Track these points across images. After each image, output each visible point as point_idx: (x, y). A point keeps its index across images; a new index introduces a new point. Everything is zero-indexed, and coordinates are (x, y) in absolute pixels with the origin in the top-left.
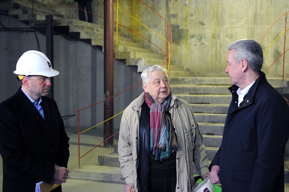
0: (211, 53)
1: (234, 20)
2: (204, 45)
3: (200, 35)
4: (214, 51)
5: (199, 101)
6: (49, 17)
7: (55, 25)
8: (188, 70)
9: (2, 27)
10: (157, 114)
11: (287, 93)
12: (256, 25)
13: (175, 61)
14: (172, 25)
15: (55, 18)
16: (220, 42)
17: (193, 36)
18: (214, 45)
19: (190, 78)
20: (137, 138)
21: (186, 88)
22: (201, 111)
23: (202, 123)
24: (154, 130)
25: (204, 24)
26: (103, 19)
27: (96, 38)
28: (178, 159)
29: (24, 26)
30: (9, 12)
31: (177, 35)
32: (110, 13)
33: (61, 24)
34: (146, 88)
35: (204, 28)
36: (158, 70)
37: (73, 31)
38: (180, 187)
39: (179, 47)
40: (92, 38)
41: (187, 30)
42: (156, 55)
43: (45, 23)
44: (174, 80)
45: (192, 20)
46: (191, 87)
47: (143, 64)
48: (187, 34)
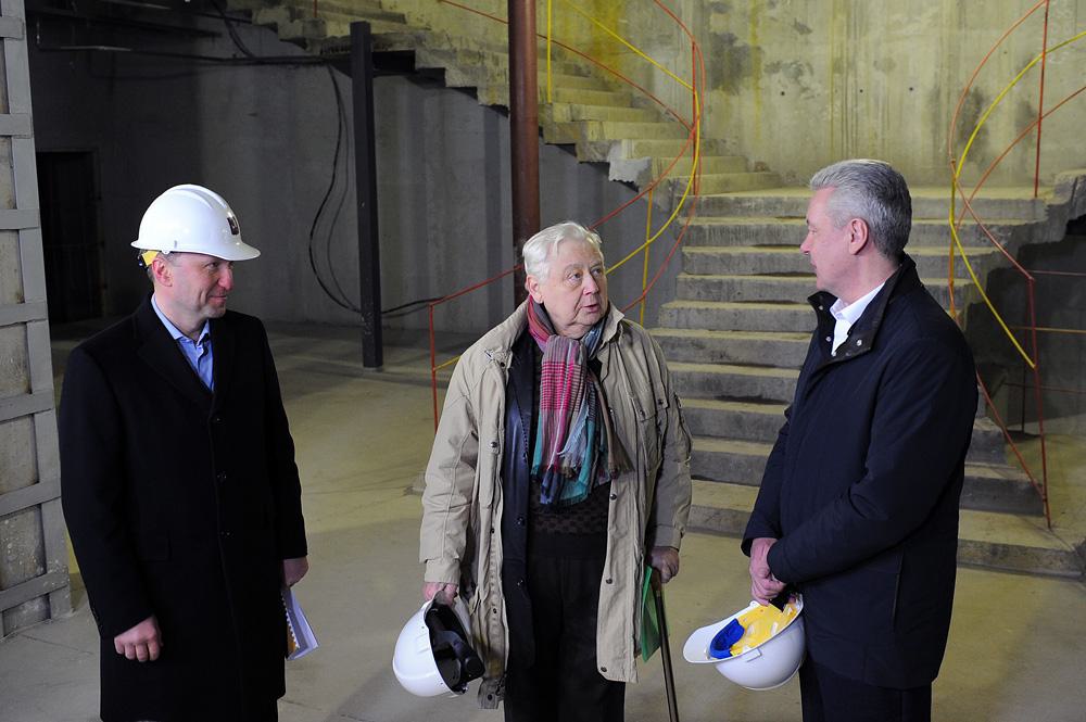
0: (830, 118)
1: (898, 16)
2: (809, 93)
3: (795, 63)
4: (836, 110)
5: (784, 267)
6: (360, 29)
7: (377, 50)
8: (761, 167)
9: (244, 56)
10: (564, 370)
11: (1045, 239)
12: (963, 31)
13: (725, 142)
14: (715, 34)
15: (378, 27)
16: (856, 82)
17: (775, 67)
18: (839, 92)
19: (761, 195)
20: (495, 445)
21: (746, 229)
22: (787, 298)
23: (787, 334)
24: (551, 418)
25: (809, 31)
26: (507, 25)
27: (490, 83)
28: (614, 497)
29: (298, 51)
30: (254, 17)
31: (727, 65)
32: (524, 13)
33: (391, 45)
34: (537, 288)
35: (807, 43)
36: (577, 240)
37: (426, 66)
38: (614, 578)
39: (734, 100)
40: (479, 84)
41: (759, 48)
42: (666, 125)
43: (349, 43)
44: (713, 203)
45: (772, 19)
46: (761, 226)
47: (624, 156)
48: (758, 61)
